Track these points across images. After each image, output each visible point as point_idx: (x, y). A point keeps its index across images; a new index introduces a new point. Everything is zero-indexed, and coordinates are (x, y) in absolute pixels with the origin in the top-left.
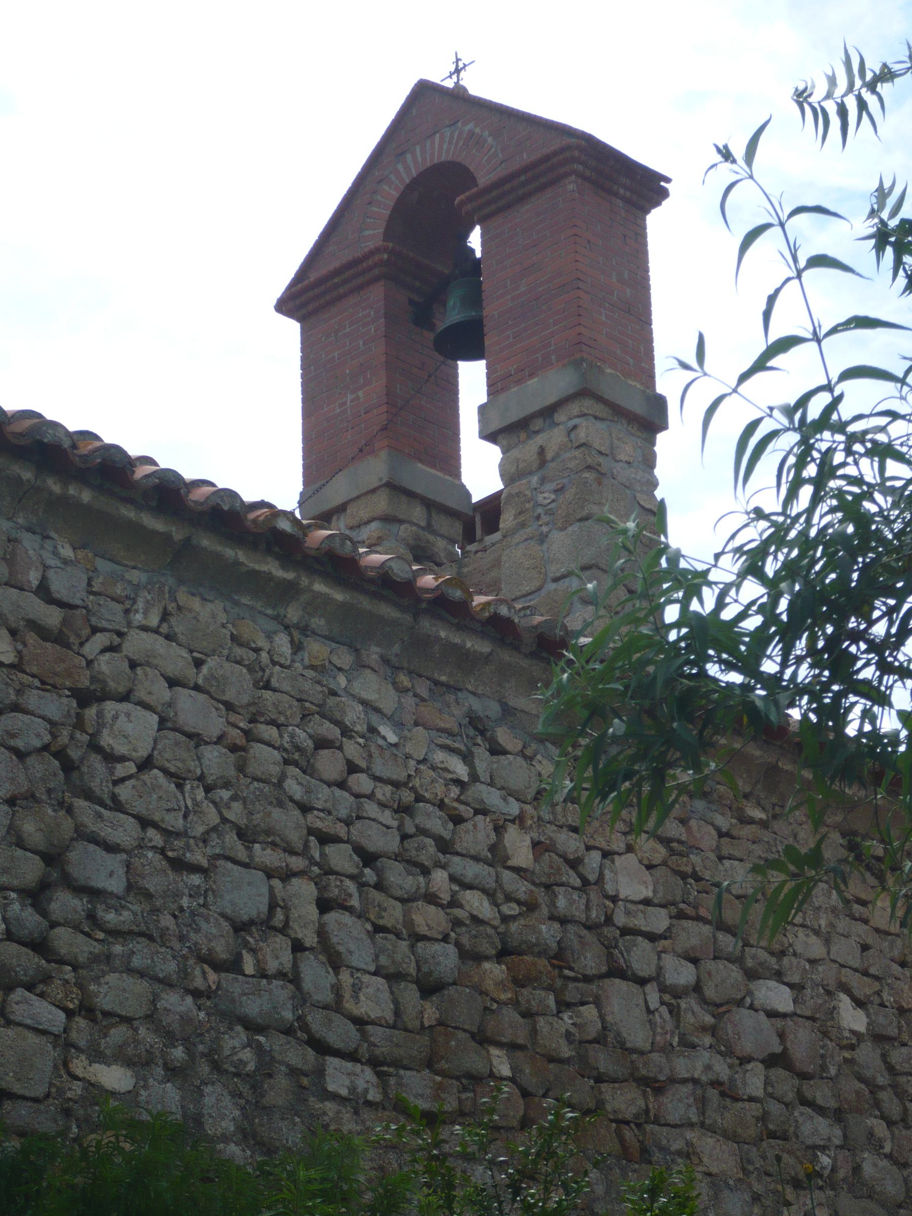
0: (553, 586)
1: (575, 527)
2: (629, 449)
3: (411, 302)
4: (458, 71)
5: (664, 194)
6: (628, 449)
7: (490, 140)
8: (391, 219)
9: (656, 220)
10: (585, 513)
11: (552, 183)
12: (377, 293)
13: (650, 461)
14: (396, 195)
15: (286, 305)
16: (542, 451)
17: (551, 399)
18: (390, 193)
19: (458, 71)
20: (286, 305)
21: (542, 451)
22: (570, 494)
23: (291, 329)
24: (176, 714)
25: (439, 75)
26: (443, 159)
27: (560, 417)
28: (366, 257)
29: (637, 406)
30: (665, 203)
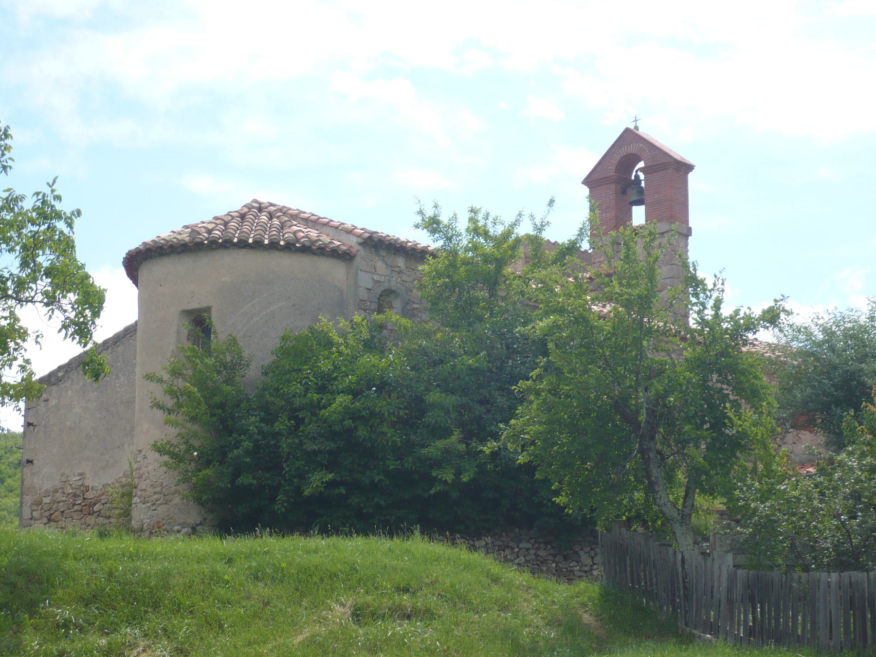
0: (663, 280)
1: (669, 266)
2: (682, 243)
3: (621, 188)
4: (636, 121)
5: (693, 169)
6: (682, 244)
7: (647, 151)
8: (617, 166)
9: (691, 176)
10: (672, 263)
11: (665, 169)
12: (613, 186)
13: (687, 245)
14: (619, 159)
15: (587, 182)
16: (660, 244)
17: (663, 231)
18: (617, 158)
19: (636, 121)
20: (587, 182)
21: (660, 244)
22: (668, 257)
23: (586, 190)
24: (774, 344)
25: (632, 127)
26: (633, 152)
27: (666, 235)
28: (610, 177)
29: (685, 232)
30: (693, 171)
